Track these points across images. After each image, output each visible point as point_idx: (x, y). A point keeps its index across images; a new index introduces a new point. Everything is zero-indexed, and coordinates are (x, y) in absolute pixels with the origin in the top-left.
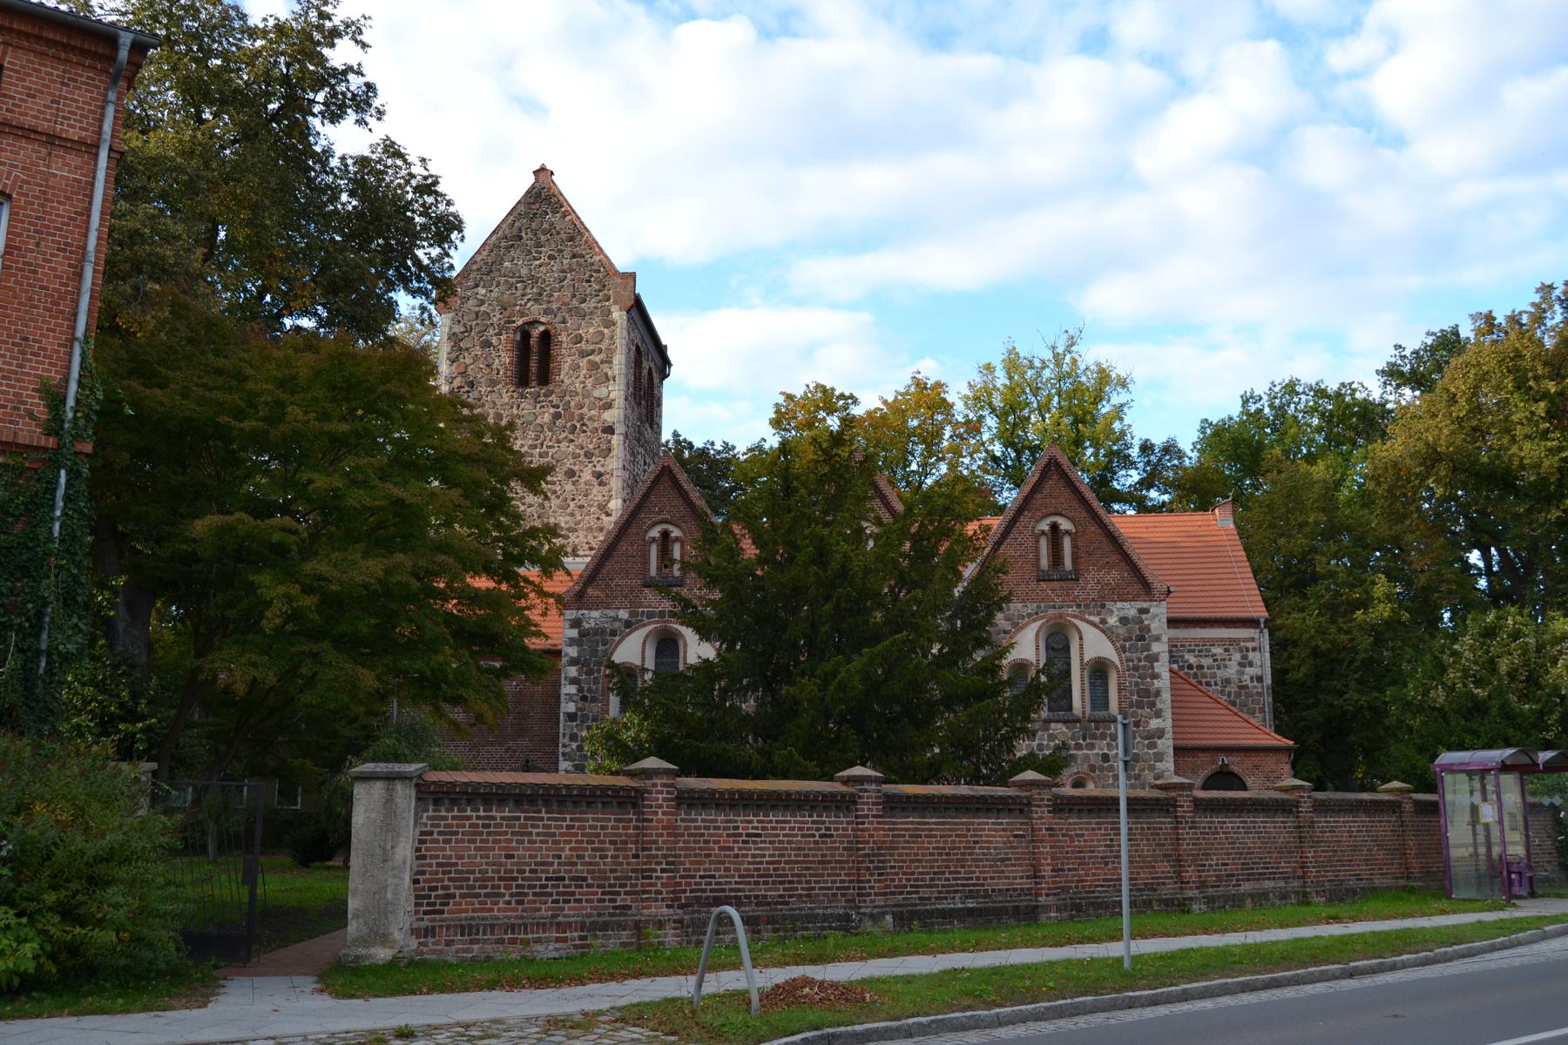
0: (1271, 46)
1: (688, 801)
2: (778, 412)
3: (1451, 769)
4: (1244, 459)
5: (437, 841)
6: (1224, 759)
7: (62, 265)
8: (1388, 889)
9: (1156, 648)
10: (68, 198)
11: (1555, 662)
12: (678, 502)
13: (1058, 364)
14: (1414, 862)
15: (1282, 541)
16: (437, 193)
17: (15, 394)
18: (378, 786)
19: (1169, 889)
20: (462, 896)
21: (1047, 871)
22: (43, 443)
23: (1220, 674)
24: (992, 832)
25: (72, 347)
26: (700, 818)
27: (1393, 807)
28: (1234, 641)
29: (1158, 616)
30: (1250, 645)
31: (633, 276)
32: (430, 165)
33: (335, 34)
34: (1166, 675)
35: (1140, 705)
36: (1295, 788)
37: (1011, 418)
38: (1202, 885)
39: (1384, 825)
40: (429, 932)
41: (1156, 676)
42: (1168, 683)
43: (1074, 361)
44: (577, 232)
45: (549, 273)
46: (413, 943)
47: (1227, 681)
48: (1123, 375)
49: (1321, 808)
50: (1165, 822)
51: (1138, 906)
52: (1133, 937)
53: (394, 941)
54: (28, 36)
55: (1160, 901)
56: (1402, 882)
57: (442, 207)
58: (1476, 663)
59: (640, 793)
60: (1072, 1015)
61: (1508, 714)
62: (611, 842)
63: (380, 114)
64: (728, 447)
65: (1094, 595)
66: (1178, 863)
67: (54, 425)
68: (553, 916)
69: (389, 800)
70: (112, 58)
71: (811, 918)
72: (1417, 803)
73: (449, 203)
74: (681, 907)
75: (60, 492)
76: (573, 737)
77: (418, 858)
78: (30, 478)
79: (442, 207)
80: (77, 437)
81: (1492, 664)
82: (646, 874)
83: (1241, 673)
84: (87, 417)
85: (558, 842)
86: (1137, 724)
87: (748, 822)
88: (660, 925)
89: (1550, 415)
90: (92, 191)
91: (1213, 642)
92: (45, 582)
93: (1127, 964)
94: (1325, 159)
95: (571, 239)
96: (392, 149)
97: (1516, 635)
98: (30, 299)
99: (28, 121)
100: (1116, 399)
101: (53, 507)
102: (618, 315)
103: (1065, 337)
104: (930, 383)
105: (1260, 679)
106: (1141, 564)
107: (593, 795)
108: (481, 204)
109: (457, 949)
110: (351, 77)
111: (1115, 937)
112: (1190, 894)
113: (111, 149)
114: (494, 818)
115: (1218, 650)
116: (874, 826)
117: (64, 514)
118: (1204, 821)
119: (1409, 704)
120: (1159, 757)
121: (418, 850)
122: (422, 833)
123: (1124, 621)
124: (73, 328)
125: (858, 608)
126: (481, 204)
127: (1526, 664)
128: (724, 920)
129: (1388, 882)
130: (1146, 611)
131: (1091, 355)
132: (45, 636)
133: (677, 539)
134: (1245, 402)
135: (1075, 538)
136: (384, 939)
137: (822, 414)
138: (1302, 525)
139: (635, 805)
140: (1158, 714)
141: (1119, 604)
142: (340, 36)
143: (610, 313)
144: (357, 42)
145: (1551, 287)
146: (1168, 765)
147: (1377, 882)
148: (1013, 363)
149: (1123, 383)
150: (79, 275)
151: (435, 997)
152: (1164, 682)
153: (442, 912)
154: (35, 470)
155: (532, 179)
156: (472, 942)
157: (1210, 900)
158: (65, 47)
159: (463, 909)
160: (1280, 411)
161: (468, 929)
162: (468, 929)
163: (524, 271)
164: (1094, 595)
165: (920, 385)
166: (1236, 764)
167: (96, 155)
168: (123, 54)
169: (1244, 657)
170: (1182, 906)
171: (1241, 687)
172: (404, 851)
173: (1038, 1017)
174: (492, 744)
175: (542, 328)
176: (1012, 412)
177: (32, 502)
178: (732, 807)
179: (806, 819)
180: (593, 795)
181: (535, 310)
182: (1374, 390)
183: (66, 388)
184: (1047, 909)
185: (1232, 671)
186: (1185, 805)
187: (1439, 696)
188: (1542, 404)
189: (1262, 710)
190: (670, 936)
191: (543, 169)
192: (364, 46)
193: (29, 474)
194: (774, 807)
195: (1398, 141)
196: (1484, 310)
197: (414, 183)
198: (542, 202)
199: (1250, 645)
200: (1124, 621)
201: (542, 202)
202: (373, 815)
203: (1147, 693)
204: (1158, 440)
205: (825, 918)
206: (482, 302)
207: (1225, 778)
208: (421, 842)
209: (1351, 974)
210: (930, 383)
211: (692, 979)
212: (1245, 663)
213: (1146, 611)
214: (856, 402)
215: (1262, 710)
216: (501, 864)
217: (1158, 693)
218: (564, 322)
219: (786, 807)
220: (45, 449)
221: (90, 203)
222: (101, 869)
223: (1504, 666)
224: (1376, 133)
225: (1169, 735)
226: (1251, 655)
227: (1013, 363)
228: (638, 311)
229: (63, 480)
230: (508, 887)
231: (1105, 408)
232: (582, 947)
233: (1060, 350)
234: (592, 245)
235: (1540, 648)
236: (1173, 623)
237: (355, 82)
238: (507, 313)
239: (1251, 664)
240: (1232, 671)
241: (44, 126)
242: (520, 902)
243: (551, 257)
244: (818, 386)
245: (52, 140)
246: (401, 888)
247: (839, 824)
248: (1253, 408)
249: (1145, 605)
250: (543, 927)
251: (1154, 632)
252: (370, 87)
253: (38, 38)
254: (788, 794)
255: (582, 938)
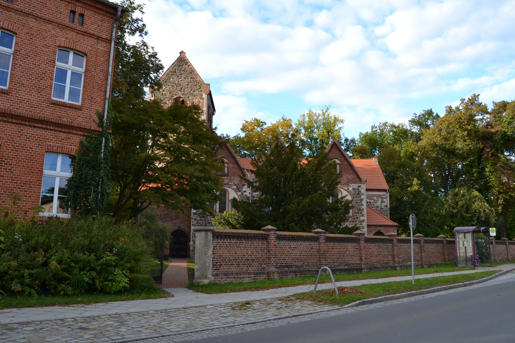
0: (359, 27)
1: (279, 238)
2: (243, 126)
3: (459, 232)
4: (372, 143)
5: (217, 249)
6: (379, 228)
7: (102, 76)
8: (441, 264)
9: (362, 197)
10: (103, 56)
11: (474, 204)
12: (226, 152)
13: (324, 114)
14: (446, 257)
15: (388, 168)
16: (156, 58)
17: (90, 115)
18: (203, 233)
19: (391, 264)
20: (224, 265)
21: (364, 258)
22: (98, 130)
23: (376, 205)
24: (350, 247)
25: (105, 101)
26: (282, 243)
27: (441, 242)
28: (379, 195)
29: (363, 188)
30: (384, 197)
31: (209, 85)
32: (154, 49)
33: (135, 9)
34: (365, 204)
35: (358, 213)
36: (420, 236)
37: (310, 130)
38: (399, 263)
39: (439, 246)
40: (217, 275)
41: (362, 205)
42: (366, 207)
43: (328, 115)
44: (192, 71)
45: (184, 83)
46: (213, 278)
47: (377, 207)
48: (342, 119)
49: (426, 242)
50: (390, 245)
51: (416, 266)
52: (415, 274)
53: (209, 278)
54: (91, 6)
55: (390, 267)
56: (444, 262)
57: (157, 62)
58: (452, 203)
59: (268, 235)
60: (412, 296)
61: (463, 217)
62: (261, 250)
63: (146, 33)
64: (227, 136)
65: (346, 182)
66: (393, 256)
67: (101, 124)
68: (247, 271)
69: (206, 237)
70: (116, 15)
71: (309, 271)
72: (448, 241)
73: (160, 61)
74: (278, 268)
75: (103, 145)
76: (195, 220)
77: (213, 254)
78: (94, 140)
79: (157, 62)
80: (107, 128)
81: (457, 203)
82: (269, 259)
83: (381, 204)
84: (110, 122)
85: (247, 250)
86: (357, 218)
87: (293, 244)
88: (274, 273)
89: (468, 135)
90: (110, 54)
91: (374, 196)
92: (101, 171)
93: (413, 283)
94: (374, 60)
95: (191, 73)
96: (144, 44)
97: (464, 196)
98: (93, 86)
99: (92, 32)
100: (340, 126)
101: (101, 149)
102: (205, 96)
103: (326, 107)
104: (287, 119)
105: (386, 206)
106: (359, 173)
107: (256, 236)
108: (167, 60)
109: (223, 280)
110: (139, 22)
111: (410, 274)
112: (396, 265)
113: (115, 42)
114: (231, 242)
115: (375, 198)
116: (324, 246)
117: (104, 151)
118: (399, 245)
119: (435, 214)
120: (363, 228)
121: (213, 251)
122: (214, 247)
123: (354, 189)
124: (105, 95)
125: (295, 184)
126: (167, 60)
127: (466, 203)
128: (325, 270)
129: (440, 262)
130: (360, 186)
131: (333, 113)
132: (100, 188)
133: (226, 162)
134: (372, 128)
135: (340, 165)
136: (206, 277)
137: (256, 127)
138: (393, 164)
139: (266, 239)
140: (363, 216)
141: (353, 184)
142: (136, 9)
143: (202, 95)
144: (141, 11)
145: (464, 99)
146: (365, 230)
147: (438, 262)
148: (310, 115)
149: (342, 122)
150: (107, 79)
151: (233, 293)
152: (364, 207)
153: (219, 269)
154: (96, 138)
155: (179, 55)
156: (227, 278)
157: (401, 267)
158: (102, 10)
159: (225, 269)
160: (382, 130)
161: (226, 274)
162: (226, 274)
163: (176, 82)
164: (346, 182)
165: (284, 120)
166: (382, 230)
167: (111, 43)
168: (119, 13)
169: (382, 200)
170: (394, 268)
171: (381, 208)
172: (210, 252)
173: (405, 296)
174: (169, 221)
175: (182, 99)
176: (309, 129)
177: (95, 147)
178: (289, 240)
179: (306, 244)
180: (256, 236)
181: (180, 94)
182: (407, 126)
183: (104, 113)
184: (364, 269)
185: (379, 204)
186: (395, 241)
187: (444, 212)
188: (466, 132)
189: (387, 215)
190: (276, 276)
191: (182, 52)
192: (143, 12)
193: (94, 139)
194: (299, 240)
195: (394, 56)
196: (449, 105)
197: (149, 54)
198: (182, 61)
199: (384, 197)
200: (354, 189)
201: (182, 61)
202: (202, 241)
203: (360, 210)
204: (350, 138)
205: (312, 271)
206: (164, 91)
207: (379, 233)
208: (214, 249)
209: (465, 285)
210: (287, 119)
211: (314, 286)
212: (383, 202)
213: (360, 186)
214: (265, 124)
215: (387, 215)
216: (234, 256)
217: (363, 210)
218: (188, 97)
219: (302, 240)
220: (99, 132)
221: (109, 58)
222: (138, 257)
223: (460, 203)
224: (387, 53)
225: (366, 221)
226: (384, 199)
227: (310, 115)
228: (210, 95)
229: (104, 141)
230: (235, 262)
231: (336, 128)
232: (254, 279)
233: (324, 111)
234: (197, 75)
235: (470, 199)
236: (367, 190)
237: (140, 24)
238: (171, 94)
239: (384, 202)
240: (379, 204)
241: (96, 34)
242: (239, 267)
243: (185, 78)
244: (255, 119)
245: (98, 38)
246: (209, 263)
247: (315, 244)
248: (374, 130)
249: (360, 185)
250: (245, 273)
251: (362, 192)
252: (144, 25)
253: (94, 7)
254: (303, 236)
255: (254, 277)
